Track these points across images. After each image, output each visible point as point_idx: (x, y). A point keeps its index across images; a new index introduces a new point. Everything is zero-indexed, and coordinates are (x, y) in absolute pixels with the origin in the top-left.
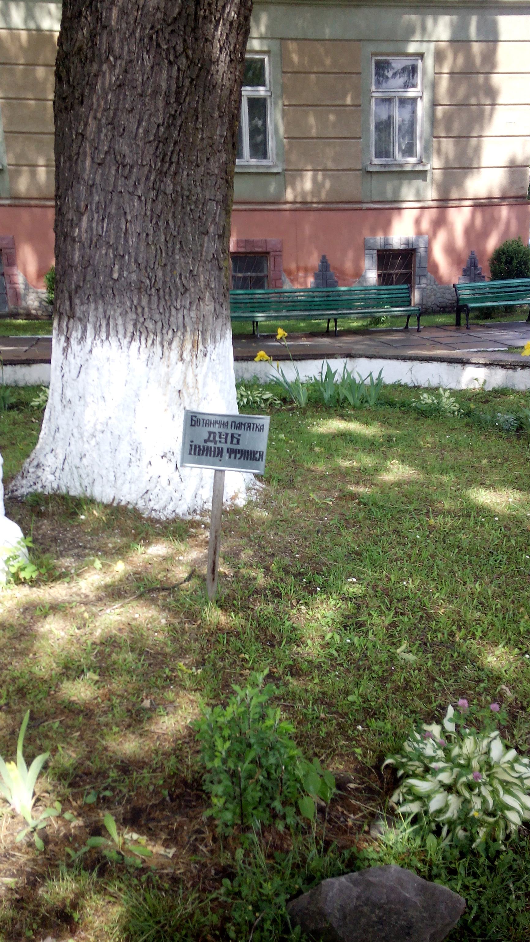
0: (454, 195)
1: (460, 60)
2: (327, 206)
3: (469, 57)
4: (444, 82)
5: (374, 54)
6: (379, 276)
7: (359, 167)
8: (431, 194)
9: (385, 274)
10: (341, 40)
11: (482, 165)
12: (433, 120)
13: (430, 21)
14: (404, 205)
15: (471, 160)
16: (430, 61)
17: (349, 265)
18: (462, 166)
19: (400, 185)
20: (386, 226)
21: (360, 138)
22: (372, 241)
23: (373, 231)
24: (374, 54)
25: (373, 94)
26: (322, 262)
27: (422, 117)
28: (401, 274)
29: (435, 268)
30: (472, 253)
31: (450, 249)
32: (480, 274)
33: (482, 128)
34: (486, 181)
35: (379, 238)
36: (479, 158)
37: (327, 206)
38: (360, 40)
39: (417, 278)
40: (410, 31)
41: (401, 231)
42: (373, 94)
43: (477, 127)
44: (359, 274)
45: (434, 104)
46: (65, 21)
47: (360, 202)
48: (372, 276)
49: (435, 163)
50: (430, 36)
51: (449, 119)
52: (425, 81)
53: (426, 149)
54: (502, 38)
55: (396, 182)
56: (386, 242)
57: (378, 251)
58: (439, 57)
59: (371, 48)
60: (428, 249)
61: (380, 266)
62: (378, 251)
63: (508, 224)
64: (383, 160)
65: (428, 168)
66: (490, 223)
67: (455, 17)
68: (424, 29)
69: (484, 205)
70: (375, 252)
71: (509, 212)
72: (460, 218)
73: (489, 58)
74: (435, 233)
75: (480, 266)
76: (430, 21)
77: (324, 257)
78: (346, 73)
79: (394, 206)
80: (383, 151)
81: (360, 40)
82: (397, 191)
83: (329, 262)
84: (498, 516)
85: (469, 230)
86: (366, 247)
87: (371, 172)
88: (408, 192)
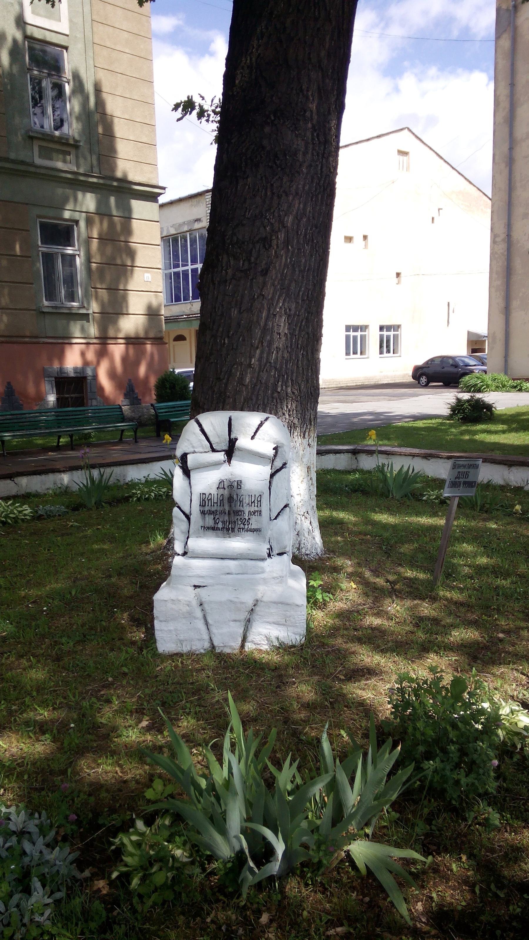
0: (111, 333)
1: (105, 224)
2: (8, 339)
3: (112, 225)
4: (95, 244)
5: (39, 217)
6: (58, 399)
7: (35, 308)
8: (93, 330)
9: (62, 398)
10: (9, 202)
11: (130, 312)
12: (89, 270)
13: (80, 195)
14: (75, 341)
15: (121, 307)
16: (82, 224)
17: (31, 389)
18: (114, 309)
19: (68, 324)
20: (61, 356)
21: (32, 284)
22: (50, 370)
23: (50, 360)
24: (39, 217)
25: (40, 249)
26: (8, 388)
27: (81, 267)
28: (76, 398)
29: (101, 389)
30: (130, 380)
31: (112, 374)
32: (137, 397)
33: (126, 282)
34: (131, 323)
35: (56, 365)
36: (127, 307)
37: (8, 339)
38: (27, 204)
39: (89, 401)
40: (66, 200)
41: (72, 360)
42: (40, 249)
43: (123, 280)
44: (41, 398)
45: (88, 260)
46: (201, 359)
47: (36, 337)
48: (52, 398)
49: (94, 307)
50: (81, 205)
51: (101, 271)
52: (81, 239)
53: (86, 295)
54: (134, 216)
55: (65, 322)
56: (61, 370)
57: (56, 378)
58: (89, 222)
59: (37, 211)
60: (95, 377)
61: (59, 392)
62: (56, 378)
63: (152, 355)
64: (52, 304)
65: (90, 312)
66: (140, 354)
67: (99, 196)
68: (76, 200)
69: (133, 341)
70: (54, 379)
71: (152, 347)
72: (117, 350)
73: (128, 230)
74: (98, 363)
75: (136, 391)
76: (80, 195)
77: (9, 383)
78: (16, 229)
79: (63, 341)
80: (51, 295)
81: (27, 204)
82: (67, 328)
83: (14, 388)
84: (229, 861)
85: (125, 359)
86: (45, 374)
87: (44, 312)
88: (76, 329)
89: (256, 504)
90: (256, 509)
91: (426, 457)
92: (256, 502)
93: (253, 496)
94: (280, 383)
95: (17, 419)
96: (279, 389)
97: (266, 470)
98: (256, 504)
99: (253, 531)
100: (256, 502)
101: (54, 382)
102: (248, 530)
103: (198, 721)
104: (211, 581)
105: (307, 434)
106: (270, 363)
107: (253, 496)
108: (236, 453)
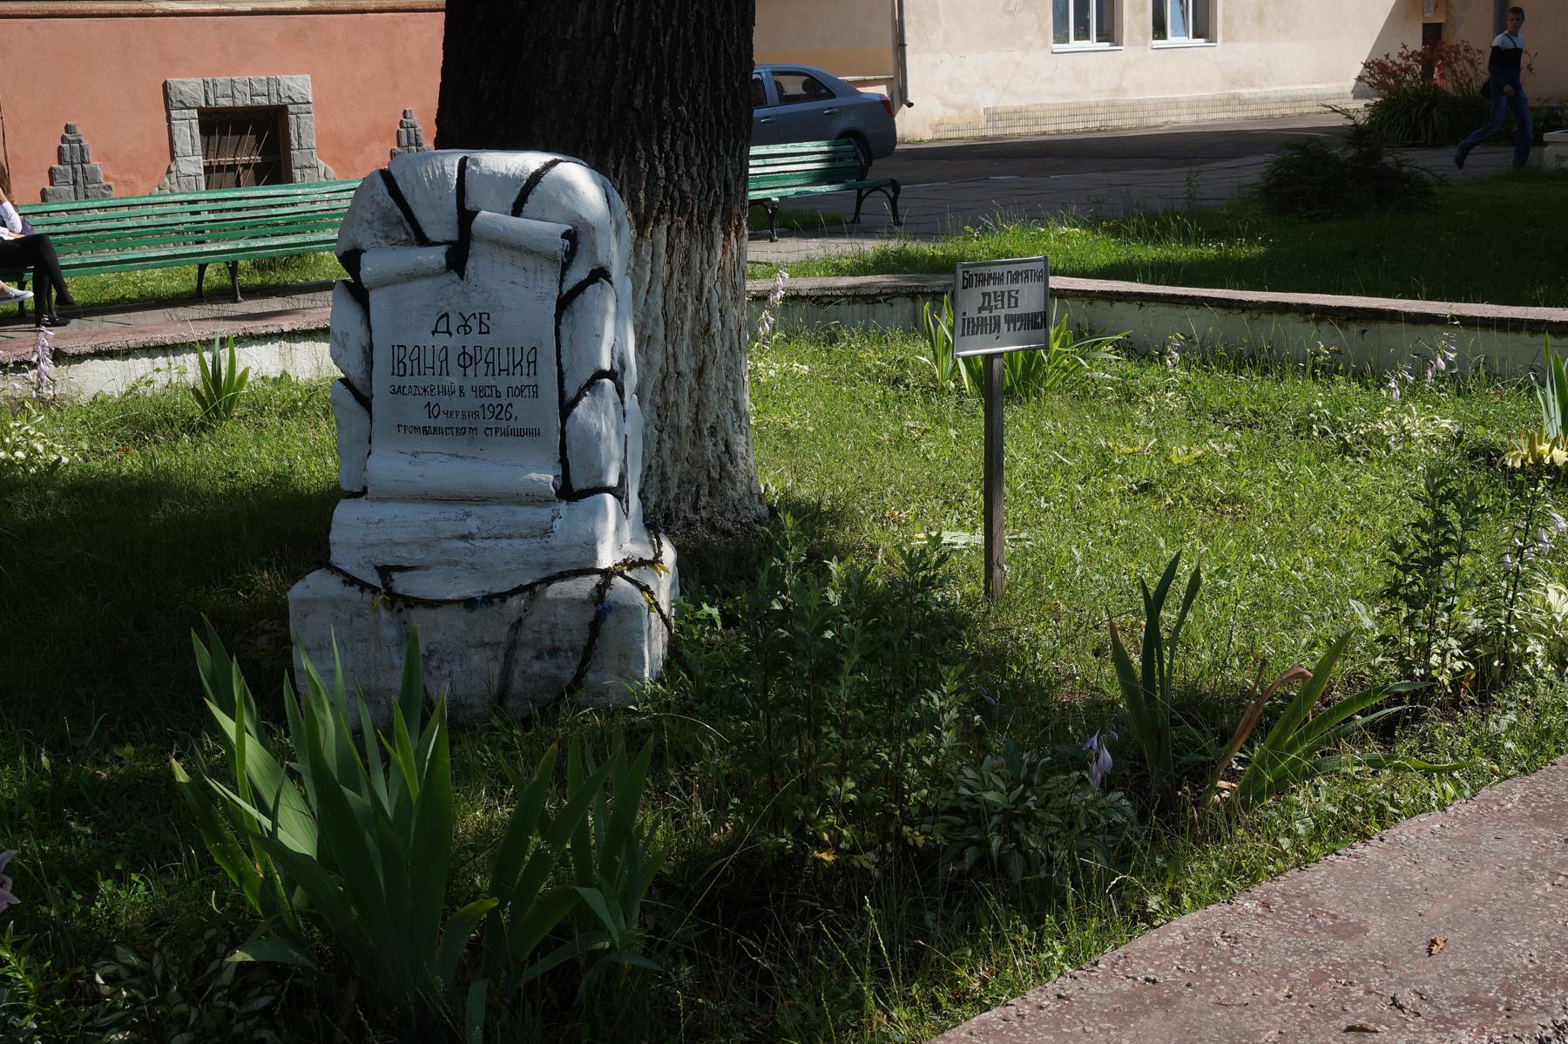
57: (200, 110)
62: (200, 110)
70: (195, 113)
89: (525, 371)
90: (525, 381)
91: (1105, 171)
92: (524, 363)
93: (518, 350)
94: (639, 87)
95: (248, 209)
96: (638, 102)
97: (548, 287)
98: (525, 371)
99: (522, 433)
100: (524, 363)
101: (195, 123)
102: (509, 433)
103: (325, 941)
104: (419, 556)
105: (985, 270)
106: (613, 35)
107: (518, 350)
108: (476, 247)
